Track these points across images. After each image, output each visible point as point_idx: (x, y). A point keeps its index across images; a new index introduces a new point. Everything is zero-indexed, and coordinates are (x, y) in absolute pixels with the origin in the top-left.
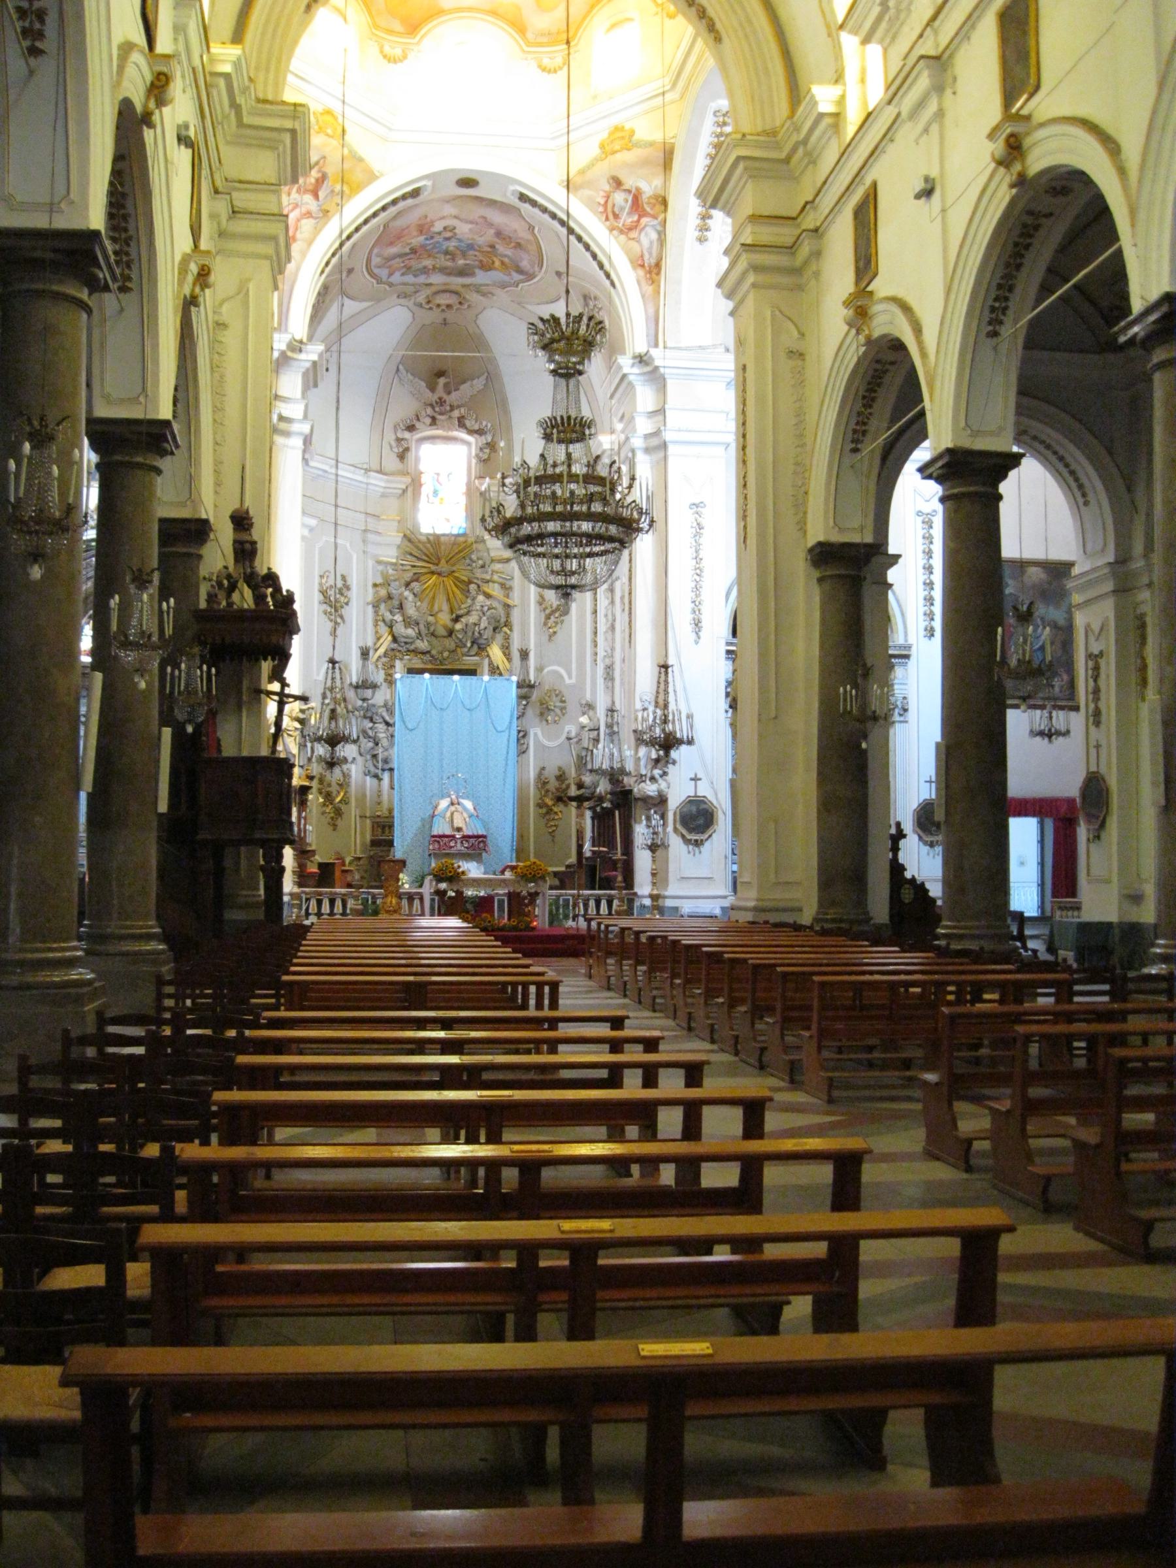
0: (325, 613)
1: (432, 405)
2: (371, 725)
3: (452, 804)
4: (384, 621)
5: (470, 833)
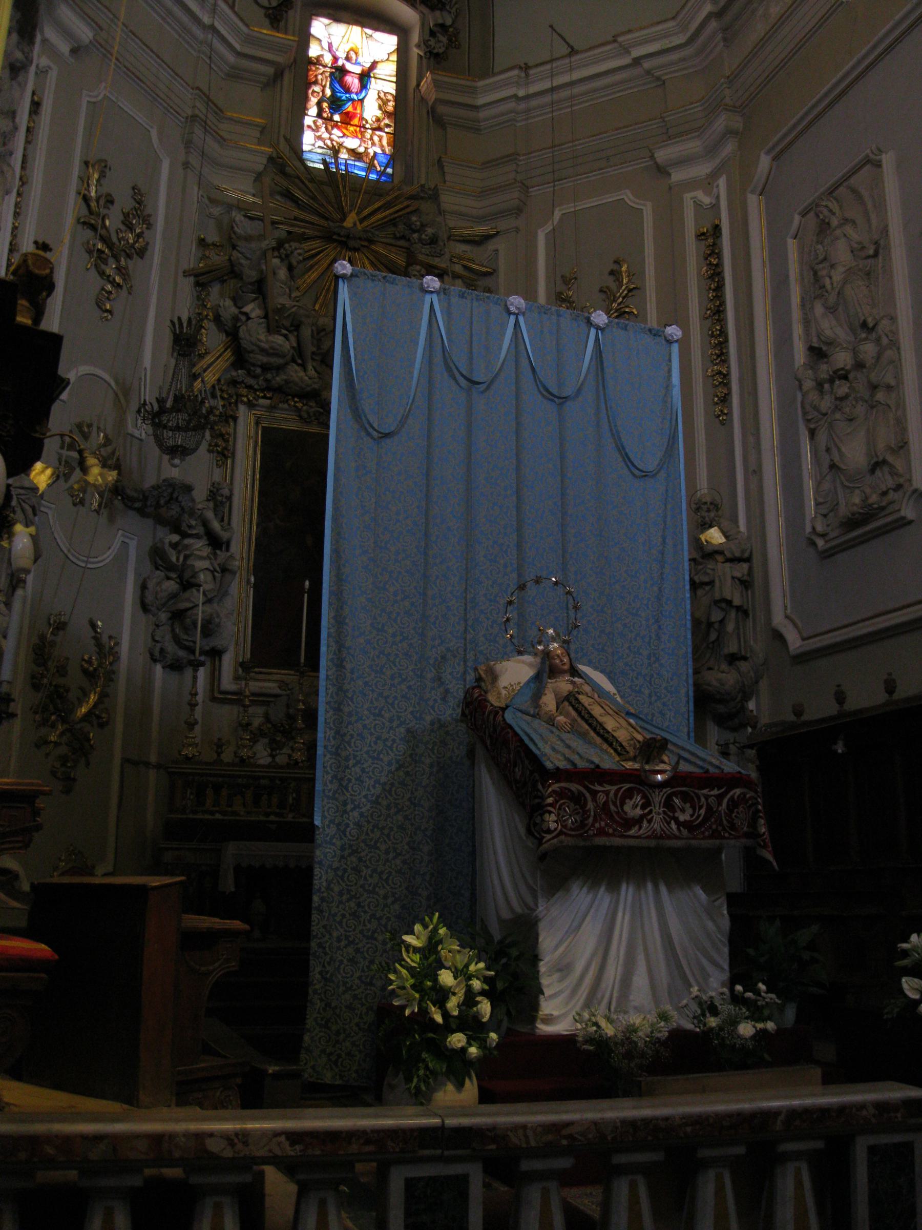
2: (175, 538)
4: (217, 319)
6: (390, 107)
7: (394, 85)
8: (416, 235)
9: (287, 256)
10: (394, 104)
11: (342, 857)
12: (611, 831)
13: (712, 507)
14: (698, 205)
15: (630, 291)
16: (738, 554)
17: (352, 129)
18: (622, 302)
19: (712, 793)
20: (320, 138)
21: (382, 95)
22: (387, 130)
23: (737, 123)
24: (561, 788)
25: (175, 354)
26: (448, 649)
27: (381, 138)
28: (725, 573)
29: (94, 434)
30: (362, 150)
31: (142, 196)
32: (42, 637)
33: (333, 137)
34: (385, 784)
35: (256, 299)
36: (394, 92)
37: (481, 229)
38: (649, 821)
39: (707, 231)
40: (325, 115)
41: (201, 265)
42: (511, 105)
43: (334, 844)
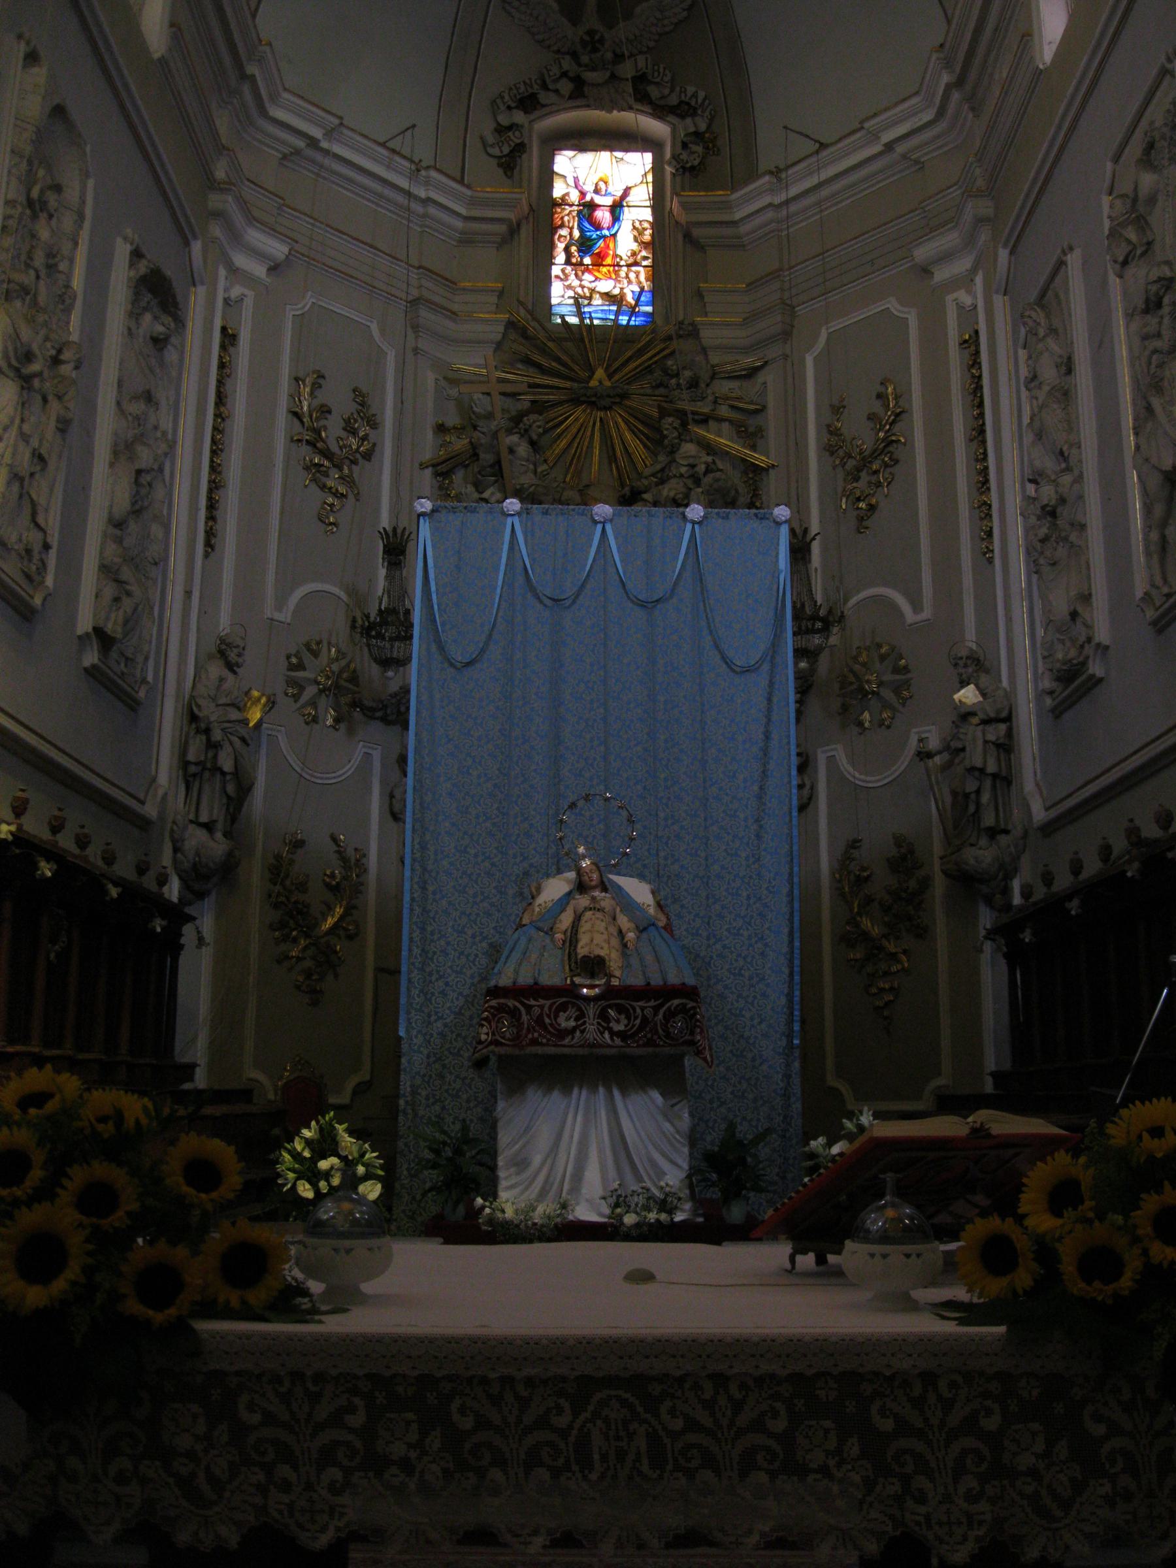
0: (310, 467)
1: (574, 55)
3: (581, 887)
5: (637, 981)
6: (647, 236)
7: (649, 210)
8: (673, 381)
9: (526, 431)
10: (651, 231)
11: (429, 1064)
12: (544, 1041)
13: (969, 662)
14: (960, 307)
15: (897, 415)
16: (992, 715)
17: (604, 270)
18: (890, 429)
19: (649, 1004)
20: (569, 287)
21: (637, 224)
22: (645, 263)
23: (985, 207)
24: (498, 1004)
25: (386, 564)
26: (531, 865)
27: (637, 274)
28: (975, 736)
29: (325, 649)
30: (616, 292)
31: (363, 397)
32: (278, 857)
33: (585, 283)
34: (468, 996)
35: (496, 481)
36: (650, 219)
37: (749, 360)
38: (582, 1032)
39: (970, 336)
40: (574, 260)
41: (441, 453)
42: (770, 214)
43: (421, 1053)
